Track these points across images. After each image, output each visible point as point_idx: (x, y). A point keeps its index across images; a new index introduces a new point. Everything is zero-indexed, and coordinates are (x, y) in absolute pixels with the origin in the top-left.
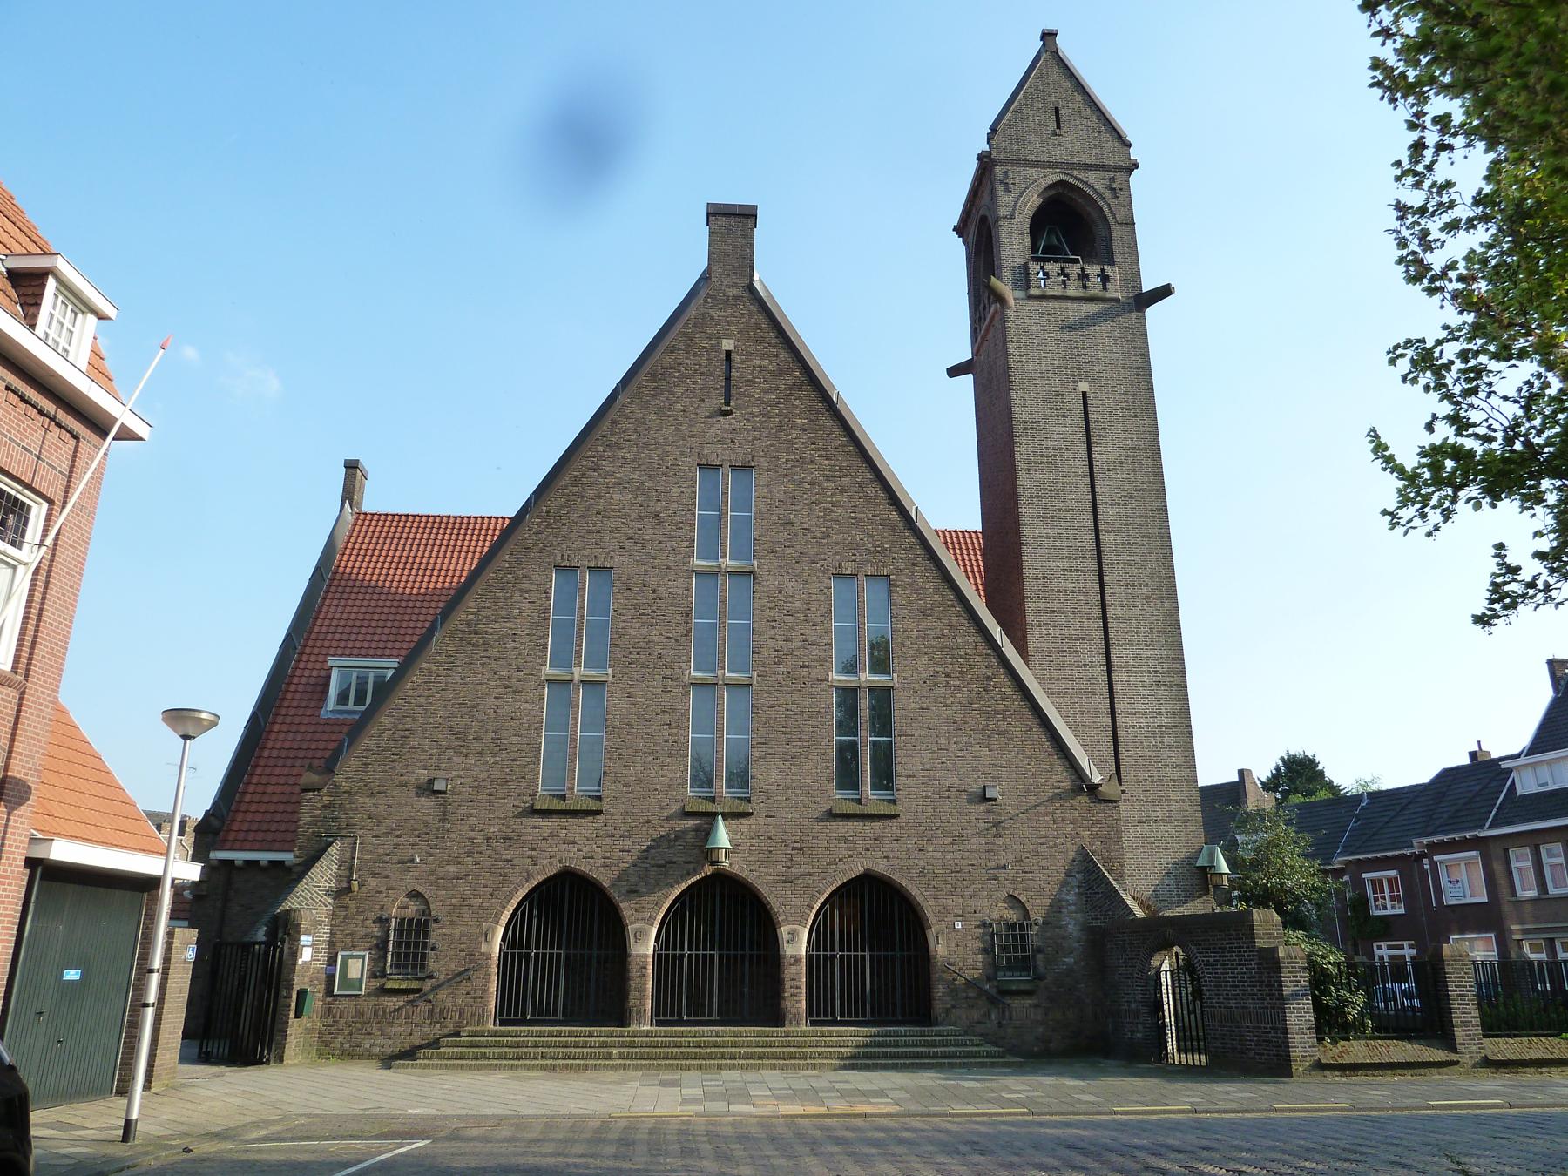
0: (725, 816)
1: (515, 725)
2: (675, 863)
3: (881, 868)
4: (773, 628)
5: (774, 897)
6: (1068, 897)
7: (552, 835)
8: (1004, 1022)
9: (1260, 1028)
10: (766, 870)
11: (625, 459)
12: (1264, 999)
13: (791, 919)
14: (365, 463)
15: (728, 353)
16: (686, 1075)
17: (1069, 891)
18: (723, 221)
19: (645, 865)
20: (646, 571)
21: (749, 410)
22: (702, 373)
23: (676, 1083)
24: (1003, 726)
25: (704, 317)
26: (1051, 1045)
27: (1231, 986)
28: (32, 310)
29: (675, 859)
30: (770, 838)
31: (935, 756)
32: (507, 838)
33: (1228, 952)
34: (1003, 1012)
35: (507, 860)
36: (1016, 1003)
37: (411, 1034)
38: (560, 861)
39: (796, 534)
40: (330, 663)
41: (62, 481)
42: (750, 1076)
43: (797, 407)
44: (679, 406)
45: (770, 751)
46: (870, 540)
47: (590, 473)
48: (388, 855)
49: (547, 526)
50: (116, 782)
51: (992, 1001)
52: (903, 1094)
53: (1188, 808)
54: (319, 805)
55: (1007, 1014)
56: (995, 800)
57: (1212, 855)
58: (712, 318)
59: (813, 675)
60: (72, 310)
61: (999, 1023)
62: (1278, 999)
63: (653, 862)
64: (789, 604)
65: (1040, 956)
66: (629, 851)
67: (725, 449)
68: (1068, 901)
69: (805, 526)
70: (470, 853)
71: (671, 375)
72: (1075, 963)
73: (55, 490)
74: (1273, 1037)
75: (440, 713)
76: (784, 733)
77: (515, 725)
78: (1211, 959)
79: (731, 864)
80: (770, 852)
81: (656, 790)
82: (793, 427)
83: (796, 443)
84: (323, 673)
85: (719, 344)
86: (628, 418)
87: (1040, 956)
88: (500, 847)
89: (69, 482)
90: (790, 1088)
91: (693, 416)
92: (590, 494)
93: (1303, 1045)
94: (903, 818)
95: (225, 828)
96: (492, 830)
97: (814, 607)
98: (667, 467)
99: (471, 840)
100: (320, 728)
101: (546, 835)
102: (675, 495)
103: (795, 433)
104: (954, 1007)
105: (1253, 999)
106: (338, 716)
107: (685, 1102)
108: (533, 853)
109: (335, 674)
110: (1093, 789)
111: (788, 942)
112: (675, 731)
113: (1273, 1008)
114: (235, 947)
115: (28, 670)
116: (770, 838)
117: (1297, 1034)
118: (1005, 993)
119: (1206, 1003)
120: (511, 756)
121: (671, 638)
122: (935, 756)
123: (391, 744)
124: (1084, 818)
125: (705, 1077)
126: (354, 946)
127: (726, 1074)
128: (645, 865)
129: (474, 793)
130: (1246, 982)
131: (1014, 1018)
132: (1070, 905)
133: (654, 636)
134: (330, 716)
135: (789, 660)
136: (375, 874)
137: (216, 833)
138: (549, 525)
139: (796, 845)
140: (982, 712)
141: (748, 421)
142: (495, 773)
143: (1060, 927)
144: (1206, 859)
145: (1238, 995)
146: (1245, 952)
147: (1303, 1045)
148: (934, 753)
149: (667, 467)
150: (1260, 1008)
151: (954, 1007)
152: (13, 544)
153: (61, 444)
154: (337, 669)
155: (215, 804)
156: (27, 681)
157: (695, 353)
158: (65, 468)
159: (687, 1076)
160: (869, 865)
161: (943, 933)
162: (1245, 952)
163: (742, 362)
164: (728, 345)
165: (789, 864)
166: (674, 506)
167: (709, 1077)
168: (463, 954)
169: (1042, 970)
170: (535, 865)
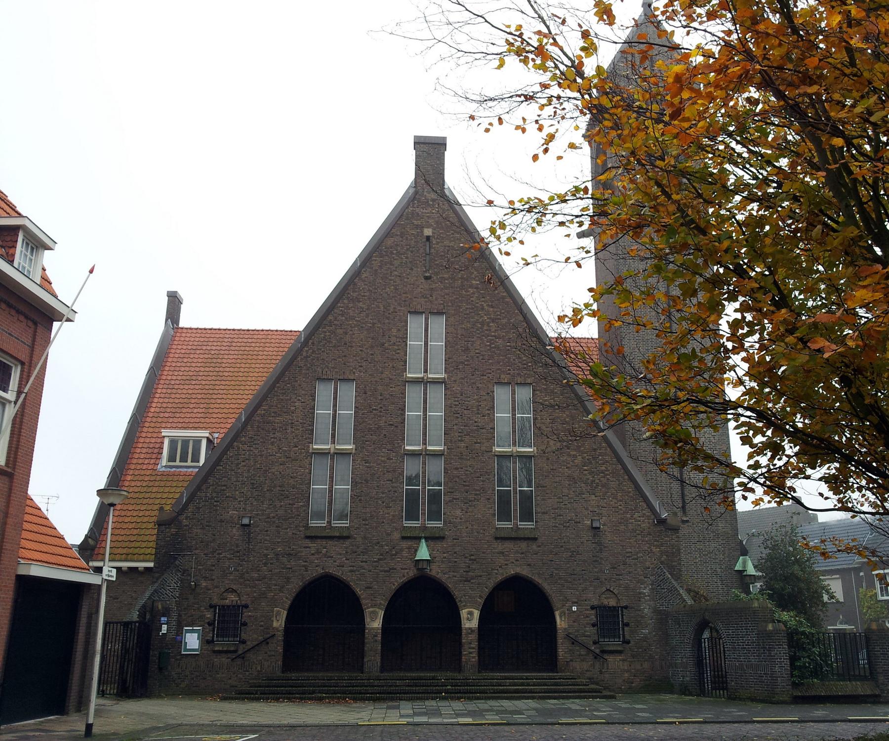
0: (427, 539)
1: (292, 481)
2: (395, 569)
3: (525, 571)
4: (457, 418)
5: (458, 591)
6: (645, 591)
7: (318, 552)
8: (603, 671)
9: (757, 674)
10: (453, 573)
11: (363, 308)
12: (761, 656)
13: (468, 605)
14: (182, 294)
15: (428, 238)
16: (402, 702)
17: (646, 587)
18: (425, 148)
19: (377, 571)
20: (376, 381)
21: (441, 276)
22: (412, 252)
23: (398, 707)
24: (604, 480)
25: (413, 214)
26: (633, 685)
27: (741, 648)
28: (11, 251)
29: (395, 567)
30: (455, 553)
31: (561, 500)
32: (290, 554)
33: (740, 627)
34: (603, 665)
35: (289, 568)
36: (610, 658)
37: (230, 679)
38: (323, 569)
39: (472, 357)
40: (163, 434)
41: (27, 350)
42: (442, 703)
43: (473, 273)
44: (396, 273)
45: (455, 497)
46: (520, 360)
47: (340, 317)
48: (214, 566)
49: (312, 353)
50: (52, 524)
51: (596, 656)
52: (533, 713)
53: (730, 532)
54: (169, 534)
55: (605, 665)
56: (599, 528)
57: (744, 563)
58: (418, 214)
59: (483, 448)
60: (31, 247)
61: (601, 671)
62: (768, 656)
63: (382, 569)
64: (467, 402)
65: (626, 628)
66: (366, 562)
67: (426, 302)
68: (645, 593)
69: (477, 351)
70: (265, 564)
71: (392, 253)
72: (649, 633)
73: (24, 357)
74: (765, 679)
75: (245, 475)
76: (465, 486)
77: (292, 481)
78: (731, 631)
79: (431, 570)
80: (456, 562)
81: (383, 522)
82: (471, 286)
83: (472, 297)
84: (159, 440)
85: (422, 232)
86: (365, 281)
87: (626, 628)
88: (285, 560)
89: (33, 351)
90: (466, 710)
91: (406, 280)
92: (340, 331)
93: (783, 684)
94: (540, 541)
95: (98, 546)
96: (279, 550)
97: (483, 404)
98: (389, 314)
99: (266, 555)
100: (158, 478)
101: (313, 552)
102: (394, 331)
103: (471, 290)
104: (572, 661)
105: (754, 656)
106: (169, 469)
107: (402, 716)
108: (305, 564)
109: (166, 442)
110: (662, 522)
111: (468, 619)
112: (394, 485)
113: (765, 662)
114: (119, 625)
115: (15, 465)
116: (455, 553)
117: (779, 677)
118: (603, 652)
119: (727, 658)
120: (291, 502)
121: (392, 425)
122: (561, 500)
123: (214, 495)
124: (656, 541)
125: (414, 704)
126: (193, 624)
127: (427, 703)
128: (377, 571)
129: (268, 526)
130: (750, 645)
131: (610, 668)
132: (646, 596)
133: (382, 424)
134: (164, 469)
135: (467, 439)
136: (206, 578)
137: (93, 549)
138: (313, 352)
139: (472, 557)
140: (591, 473)
141: (441, 282)
142: (281, 512)
143: (640, 610)
144: (741, 565)
145: (746, 653)
146: (750, 627)
147: (783, 684)
148: (560, 498)
149: (389, 314)
150: (758, 662)
151: (572, 661)
152: (4, 391)
153: (27, 328)
154: (168, 438)
155: (91, 530)
156: (14, 471)
157: (407, 238)
158: (29, 343)
159: (403, 703)
160: (518, 570)
161: (565, 614)
162: (750, 627)
163: (438, 243)
164: (428, 232)
165: (467, 570)
166: (393, 340)
167: (417, 704)
168: (262, 628)
169: (627, 637)
170: (307, 571)
